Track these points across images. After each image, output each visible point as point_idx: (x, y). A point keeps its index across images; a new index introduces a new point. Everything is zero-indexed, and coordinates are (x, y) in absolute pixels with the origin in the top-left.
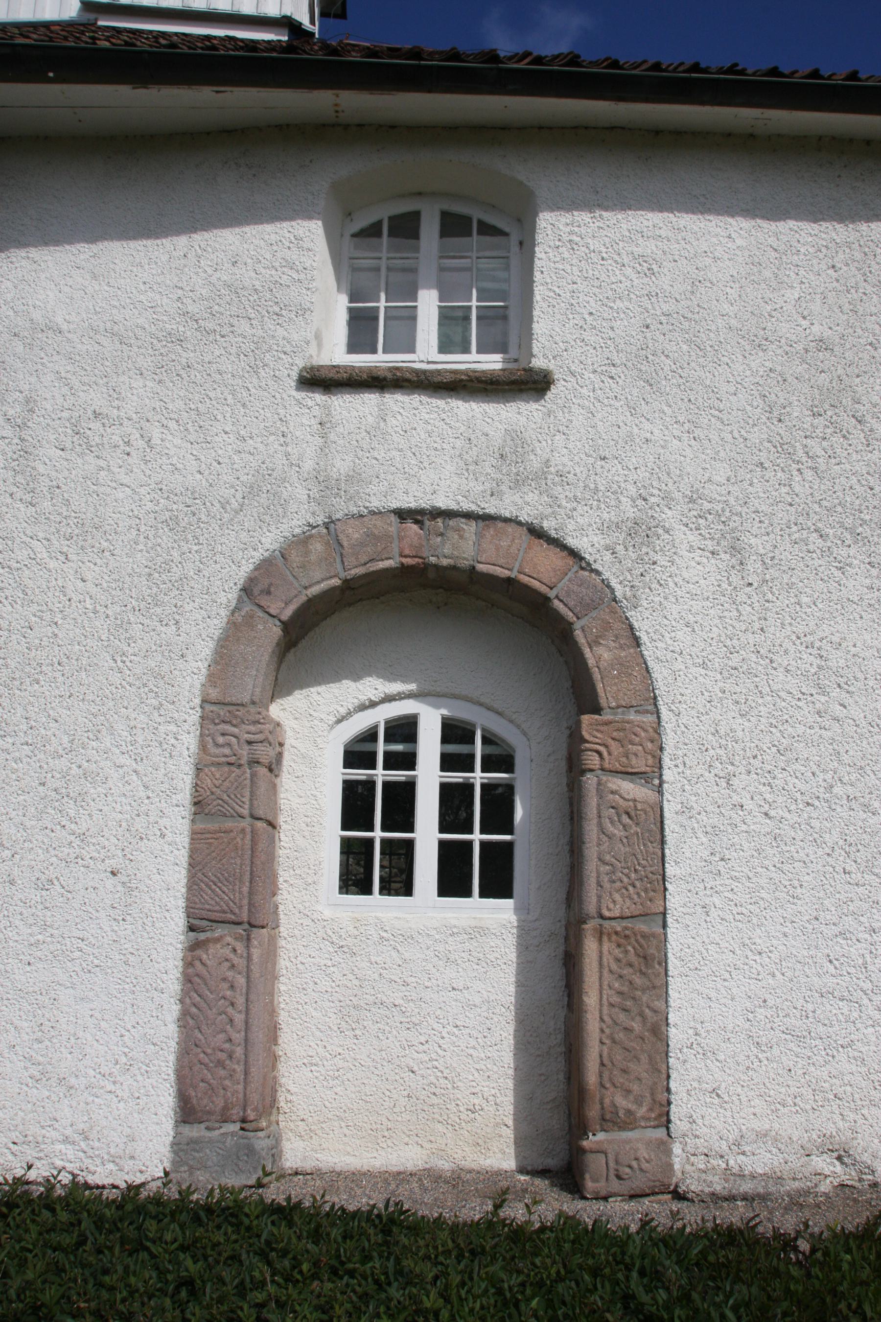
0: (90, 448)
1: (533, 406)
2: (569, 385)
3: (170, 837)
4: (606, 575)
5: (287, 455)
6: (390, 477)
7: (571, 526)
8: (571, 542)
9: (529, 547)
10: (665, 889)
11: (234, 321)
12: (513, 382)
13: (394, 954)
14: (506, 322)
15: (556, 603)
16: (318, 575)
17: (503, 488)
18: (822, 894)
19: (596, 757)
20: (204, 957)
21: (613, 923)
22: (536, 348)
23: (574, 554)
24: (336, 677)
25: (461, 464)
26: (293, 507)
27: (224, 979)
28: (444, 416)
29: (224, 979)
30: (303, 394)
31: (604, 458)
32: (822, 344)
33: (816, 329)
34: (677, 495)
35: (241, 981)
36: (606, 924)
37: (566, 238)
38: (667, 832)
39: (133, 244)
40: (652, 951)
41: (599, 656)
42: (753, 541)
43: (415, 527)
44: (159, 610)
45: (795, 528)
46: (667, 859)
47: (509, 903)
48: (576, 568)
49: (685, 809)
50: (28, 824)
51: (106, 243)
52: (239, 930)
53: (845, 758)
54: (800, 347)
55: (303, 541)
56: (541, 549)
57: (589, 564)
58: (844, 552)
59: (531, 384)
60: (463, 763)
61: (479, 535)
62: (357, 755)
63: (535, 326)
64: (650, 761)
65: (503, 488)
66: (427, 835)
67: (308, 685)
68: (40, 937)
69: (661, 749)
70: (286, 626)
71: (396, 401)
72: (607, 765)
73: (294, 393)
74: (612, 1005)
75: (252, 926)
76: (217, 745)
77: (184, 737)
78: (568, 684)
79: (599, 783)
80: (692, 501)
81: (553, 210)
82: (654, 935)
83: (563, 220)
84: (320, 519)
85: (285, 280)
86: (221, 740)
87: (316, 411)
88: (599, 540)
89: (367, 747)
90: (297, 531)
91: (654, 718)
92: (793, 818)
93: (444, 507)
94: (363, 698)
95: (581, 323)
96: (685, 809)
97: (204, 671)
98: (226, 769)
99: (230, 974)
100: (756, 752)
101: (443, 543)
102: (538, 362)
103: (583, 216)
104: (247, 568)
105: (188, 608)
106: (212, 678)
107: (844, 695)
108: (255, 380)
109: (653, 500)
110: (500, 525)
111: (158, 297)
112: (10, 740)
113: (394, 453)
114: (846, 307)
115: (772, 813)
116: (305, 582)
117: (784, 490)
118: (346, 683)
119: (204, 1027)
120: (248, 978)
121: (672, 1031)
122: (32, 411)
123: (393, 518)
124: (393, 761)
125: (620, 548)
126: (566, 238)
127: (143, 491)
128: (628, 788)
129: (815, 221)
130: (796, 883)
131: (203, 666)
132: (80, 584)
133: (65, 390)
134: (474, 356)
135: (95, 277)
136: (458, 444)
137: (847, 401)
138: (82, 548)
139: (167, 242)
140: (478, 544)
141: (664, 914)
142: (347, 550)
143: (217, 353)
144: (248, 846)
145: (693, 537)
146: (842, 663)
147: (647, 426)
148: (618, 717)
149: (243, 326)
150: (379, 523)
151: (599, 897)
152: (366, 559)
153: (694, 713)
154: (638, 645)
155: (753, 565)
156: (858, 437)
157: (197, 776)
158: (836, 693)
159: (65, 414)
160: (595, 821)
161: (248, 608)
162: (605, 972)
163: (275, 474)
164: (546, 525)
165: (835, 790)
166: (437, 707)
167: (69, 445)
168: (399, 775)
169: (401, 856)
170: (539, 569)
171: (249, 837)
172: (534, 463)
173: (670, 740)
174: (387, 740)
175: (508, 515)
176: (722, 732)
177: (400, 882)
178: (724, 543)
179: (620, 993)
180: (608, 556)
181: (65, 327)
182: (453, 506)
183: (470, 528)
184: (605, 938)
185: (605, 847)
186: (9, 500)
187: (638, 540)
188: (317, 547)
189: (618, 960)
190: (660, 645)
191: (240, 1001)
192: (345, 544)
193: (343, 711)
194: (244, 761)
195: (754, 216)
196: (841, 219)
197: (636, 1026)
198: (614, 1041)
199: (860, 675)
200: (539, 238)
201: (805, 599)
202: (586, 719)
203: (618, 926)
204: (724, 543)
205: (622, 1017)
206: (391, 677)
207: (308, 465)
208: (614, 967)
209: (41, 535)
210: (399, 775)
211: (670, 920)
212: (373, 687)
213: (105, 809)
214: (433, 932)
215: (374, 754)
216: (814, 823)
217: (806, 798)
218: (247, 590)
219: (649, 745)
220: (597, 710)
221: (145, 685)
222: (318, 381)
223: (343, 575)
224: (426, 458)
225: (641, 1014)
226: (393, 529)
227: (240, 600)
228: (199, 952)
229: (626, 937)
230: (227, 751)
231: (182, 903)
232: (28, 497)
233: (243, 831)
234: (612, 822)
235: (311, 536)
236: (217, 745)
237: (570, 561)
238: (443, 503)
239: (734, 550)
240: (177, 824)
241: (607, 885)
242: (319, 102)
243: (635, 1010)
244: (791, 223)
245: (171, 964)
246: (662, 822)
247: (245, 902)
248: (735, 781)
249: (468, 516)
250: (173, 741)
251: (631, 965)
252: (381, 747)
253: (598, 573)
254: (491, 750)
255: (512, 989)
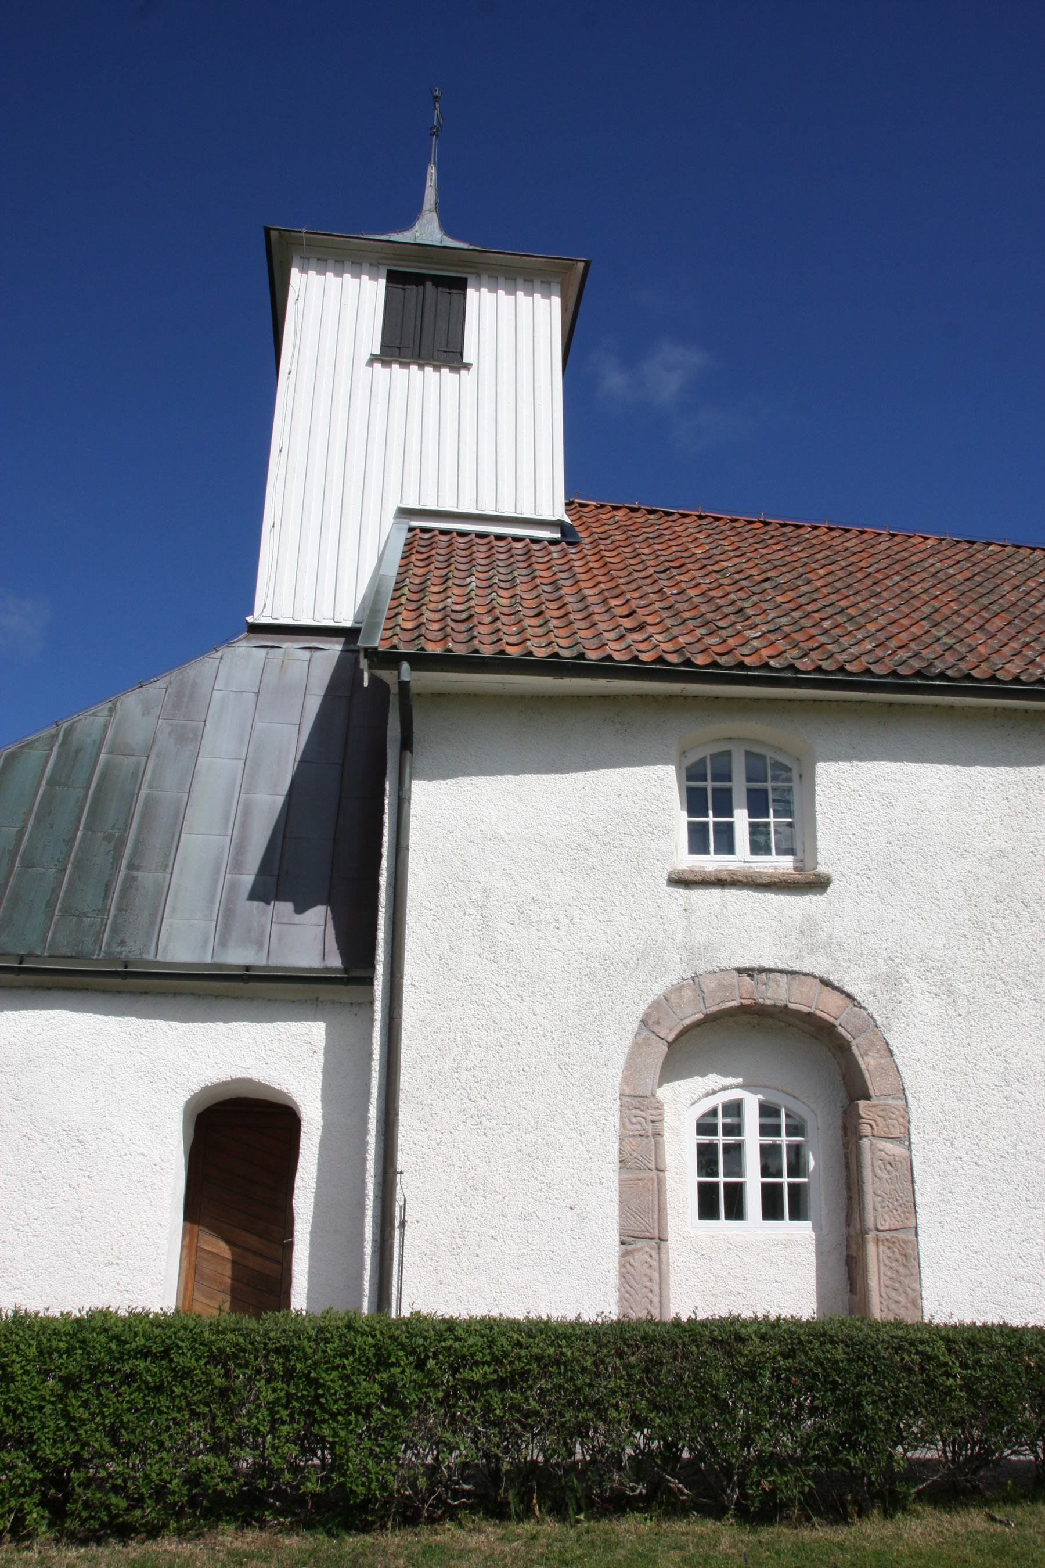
0: (531, 923)
1: (819, 897)
2: (842, 883)
3: (606, 1184)
4: (870, 1010)
5: (665, 931)
6: (732, 946)
7: (847, 978)
8: (848, 989)
9: (821, 993)
10: (916, 1212)
11: (622, 837)
12: (808, 883)
13: (737, 1259)
14: (797, 840)
15: (840, 1029)
16: (689, 1012)
17: (804, 953)
18: (1013, 1214)
19: (869, 1127)
20: (632, 1261)
21: (885, 1234)
22: (820, 858)
23: (849, 996)
24: (689, 1075)
25: (776, 937)
26: (672, 967)
27: (645, 1275)
28: (763, 904)
29: (645, 1275)
30: (672, 889)
31: (865, 933)
32: (1002, 853)
33: (997, 842)
34: (912, 957)
35: (656, 1275)
36: (880, 1234)
37: (835, 780)
38: (915, 1175)
39: (545, 777)
40: (909, 1251)
41: (868, 1063)
42: (961, 986)
43: (748, 979)
44: (587, 1035)
45: (987, 977)
46: (916, 1192)
47: (808, 1224)
48: (851, 1005)
49: (926, 1161)
50: (512, 1177)
51: (526, 776)
52: (653, 1242)
53: (1023, 1126)
54: (987, 856)
55: (679, 989)
56: (828, 994)
57: (859, 1003)
58: (1018, 992)
59: (819, 884)
60: (775, 1131)
61: (789, 984)
62: (705, 1127)
63: (818, 842)
64: (902, 1130)
65: (804, 953)
66: (753, 1181)
67: (672, 1081)
68: (525, 1251)
69: (909, 1122)
70: (670, 1044)
71: (732, 894)
72: (876, 1133)
73: (666, 888)
74: (887, 1286)
75: (660, 1239)
76: (632, 1123)
77: (611, 1118)
78: (840, 1078)
79: (871, 1145)
80: (922, 961)
81: (825, 761)
82: (910, 1241)
83: (833, 768)
84: (689, 975)
85: (654, 808)
86: (634, 1120)
87: (681, 901)
88: (865, 988)
89: (709, 1120)
90: (675, 982)
91: (903, 1102)
92: (993, 1166)
93: (767, 966)
94: (709, 1089)
95: (848, 841)
96: (926, 1161)
97: (620, 1075)
98: (639, 1139)
99: (648, 1271)
100: (968, 1123)
101: (767, 990)
102: (822, 869)
103: (845, 765)
104: (644, 1007)
105: (606, 1033)
106: (625, 1080)
107: (1022, 1086)
108: (640, 879)
109: (897, 960)
110: (802, 977)
111: (569, 818)
112: (494, 1122)
113: (734, 930)
114: (1016, 827)
115: (980, 1163)
116: (681, 1016)
117: (980, 952)
118: (697, 1078)
119: (634, 1306)
120: (660, 1273)
121: (925, 1302)
122: (488, 896)
123: (735, 973)
124: (729, 1130)
125: (878, 993)
126: (835, 780)
127: (570, 954)
128: (889, 1147)
129: (994, 766)
130: (997, 1207)
131: (619, 1072)
132: (532, 1016)
133: (510, 882)
134: (774, 857)
135: (521, 800)
136: (774, 923)
137: (1018, 892)
138: (532, 992)
139: (568, 776)
140: (789, 990)
141: (916, 1228)
142: (707, 995)
143: (612, 859)
144: (656, 1189)
145: (923, 984)
146: (1019, 1065)
147: (892, 911)
148: (882, 1102)
149: (628, 841)
150: (726, 977)
151: (875, 1217)
152: (719, 1000)
153: (928, 1099)
154: (892, 1055)
155: (962, 1002)
156: (1025, 915)
157: (621, 1144)
158: (1016, 1084)
159: (513, 899)
160: (870, 1169)
161: (645, 1033)
162: (881, 1265)
163: (658, 944)
164: (831, 978)
165: (1019, 1147)
166: (755, 1093)
167: (517, 922)
168: (731, 1139)
169: (735, 1194)
170: (828, 1007)
171: (656, 1184)
172: (822, 936)
173: (914, 1116)
174: (724, 1116)
175: (807, 971)
176: (946, 1111)
177: (736, 1211)
178: (943, 988)
179: (891, 1279)
180: (871, 998)
181: (506, 837)
182: (773, 966)
183: (783, 979)
184: (880, 1243)
185: (877, 1185)
186: (478, 958)
187: (889, 987)
188: (688, 993)
189: (889, 1258)
190: (905, 1055)
191: (656, 1288)
192: (705, 991)
193: (696, 1097)
194: (650, 1134)
195: (955, 764)
196: (1011, 764)
197: (902, 1299)
198: (889, 1310)
199: (1030, 1073)
200: (818, 780)
201: (995, 1024)
202: (862, 1103)
203: (888, 1235)
204: (943, 988)
205: (893, 1294)
206: (726, 1075)
207: (679, 938)
208: (887, 1261)
209: (503, 983)
210: (731, 1139)
211: (919, 1231)
212: (714, 1080)
213: (562, 1166)
214: (761, 1244)
215: (715, 1126)
216: (1005, 1168)
217: (1001, 1153)
218: (643, 1022)
219: (901, 1120)
220: (868, 1097)
221: (582, 1085)
222: (681, 881)
223: (705, 1011)
224: (752, 934)
225: (905, 1293)
226: (735, 981)
227: (640, 1028)
228: (628, 1258)
229: (893, 1242)
230: (638, 1127)
231: (616, 1226)
232: (491, 957)
233: (652, 1179)
234: (880, 1169)
235: (683, 986)
236: (632, 1123)
237: (847, 1001)
238: (766, 964)
239: (949, 992)
240: (611, 1174)
241: (879, 1209)
242: (675, 687)
243: (901, 1290)
244: (979, 768)
245: (611, 1266)
246: (912, 1169)
247: (656, 1225)
248: (956, 1143)
249: (782, 972)
250: (604, 1121)
251: (897, 1261)
252: (720, 1121)
253: (865, 1009)
254: (791, 1122)
255: (814, 1281)
